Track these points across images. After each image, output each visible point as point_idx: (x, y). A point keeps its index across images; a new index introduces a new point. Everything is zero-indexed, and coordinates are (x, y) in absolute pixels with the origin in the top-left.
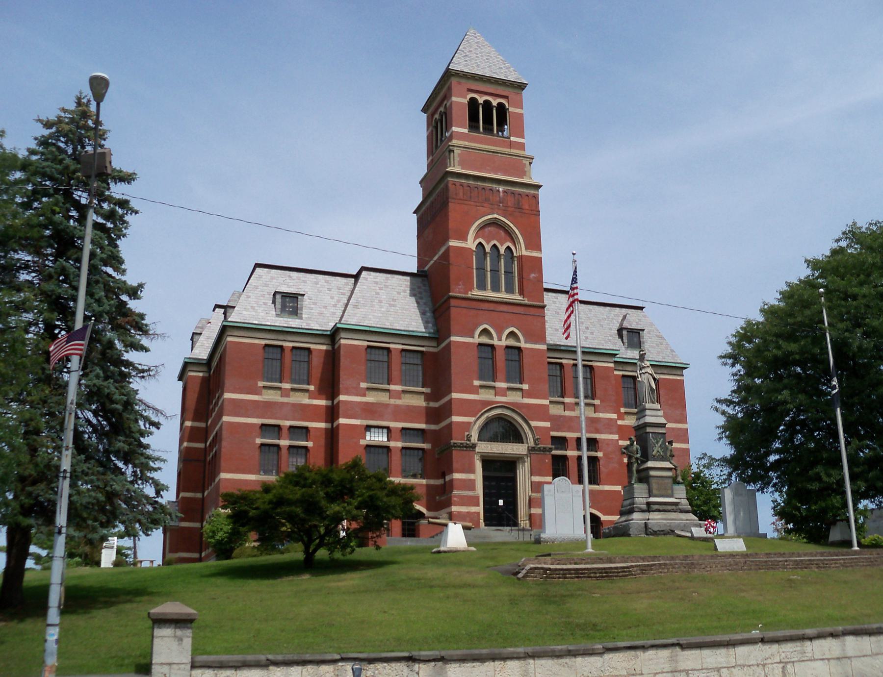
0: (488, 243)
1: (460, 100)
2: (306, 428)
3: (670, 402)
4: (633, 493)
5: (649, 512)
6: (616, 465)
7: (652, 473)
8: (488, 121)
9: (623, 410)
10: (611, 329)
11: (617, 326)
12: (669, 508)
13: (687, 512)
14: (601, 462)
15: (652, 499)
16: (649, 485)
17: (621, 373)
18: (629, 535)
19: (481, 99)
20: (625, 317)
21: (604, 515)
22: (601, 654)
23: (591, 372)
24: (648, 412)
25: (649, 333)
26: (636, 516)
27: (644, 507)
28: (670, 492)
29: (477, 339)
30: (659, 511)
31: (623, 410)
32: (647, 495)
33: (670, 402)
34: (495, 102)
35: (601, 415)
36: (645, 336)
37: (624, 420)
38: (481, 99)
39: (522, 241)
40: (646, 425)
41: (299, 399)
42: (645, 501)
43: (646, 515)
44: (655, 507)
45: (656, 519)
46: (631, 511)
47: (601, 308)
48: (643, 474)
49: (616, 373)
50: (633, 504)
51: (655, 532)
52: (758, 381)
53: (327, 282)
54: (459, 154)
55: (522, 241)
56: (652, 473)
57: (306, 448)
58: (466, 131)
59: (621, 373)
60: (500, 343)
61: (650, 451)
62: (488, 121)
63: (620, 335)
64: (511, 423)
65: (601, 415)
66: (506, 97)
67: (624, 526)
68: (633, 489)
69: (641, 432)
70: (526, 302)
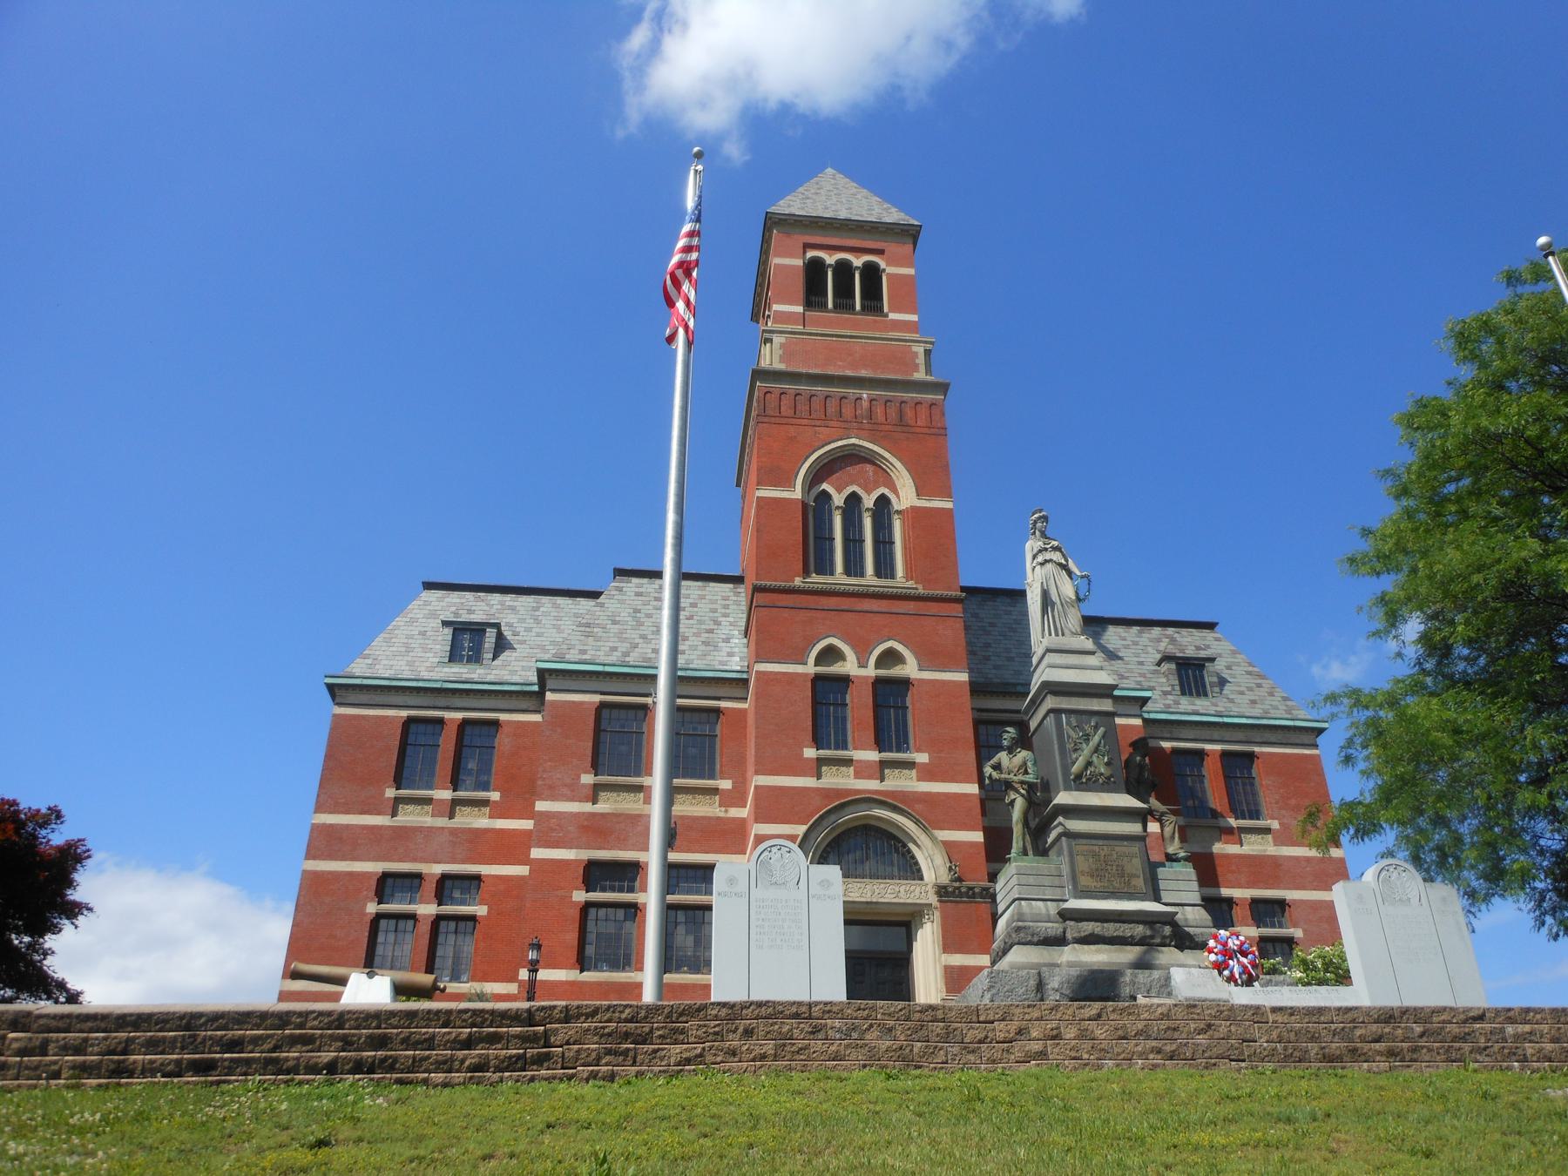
0: (839, 491)
1: (788, 261)
2: (477, 878)
3: (1293, 802)
8: (844, 291)
19: (830, 259)
22: (1405, 1011)
29: (810, 668)
33: (1293, 802)
34: (858, 261)
38: (830, 259)
39: (887, 455)
41: (468, 820)
52: (1546, 500)
53: (556, 606)
54: (782, 346)
55: (887, 455)
57: (472, 918)
58: (800, 309)
60: (863, 672)
62: (844, 291)
64: (856, 828)
66: (880, 252)
70: (921, 591)
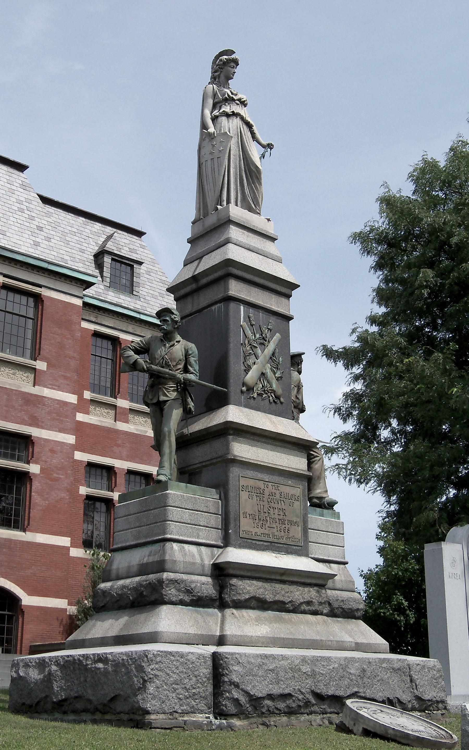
4: (163, 520)
5: (222, 604)
6: (64, 495)
7: (242, 450)
9: (87, 395)
10: (82, 251)
11: (96, 249)
12: (298, 594)
13: (348, 614)
14: (36, 485)
15: (237, 555)
16: (225, 498)
17: (92, 327)
18: (137, 719)
20: (110, 237)
21: (29, 594)
23: (36, 307)
24: (234, 233)
25: (148, 273)
26: (169, 620)
27: (204, 584)
28: (297, 532)
30: (261, 604)
31: (87, 395)
32: (214, 537)
35: (47, 392)
36: (140, 270)
37: (87, 413)
40: (230, 270)
42: (206, 558)
43: (209, 621)
44: (247, 588)
45: (251, 636)
46: (147, 599)
47: (70, 217)
48: (199, 454)
49: (85, 325)
50: (160, 566)
51: (255, 701)
56: (242, 450)
59: (92, 327)
61: (235, 366)
63: (99, 266)
65: (47, 392)
67: (118, 665)
68: (163, 504)
69: (203, 299)
